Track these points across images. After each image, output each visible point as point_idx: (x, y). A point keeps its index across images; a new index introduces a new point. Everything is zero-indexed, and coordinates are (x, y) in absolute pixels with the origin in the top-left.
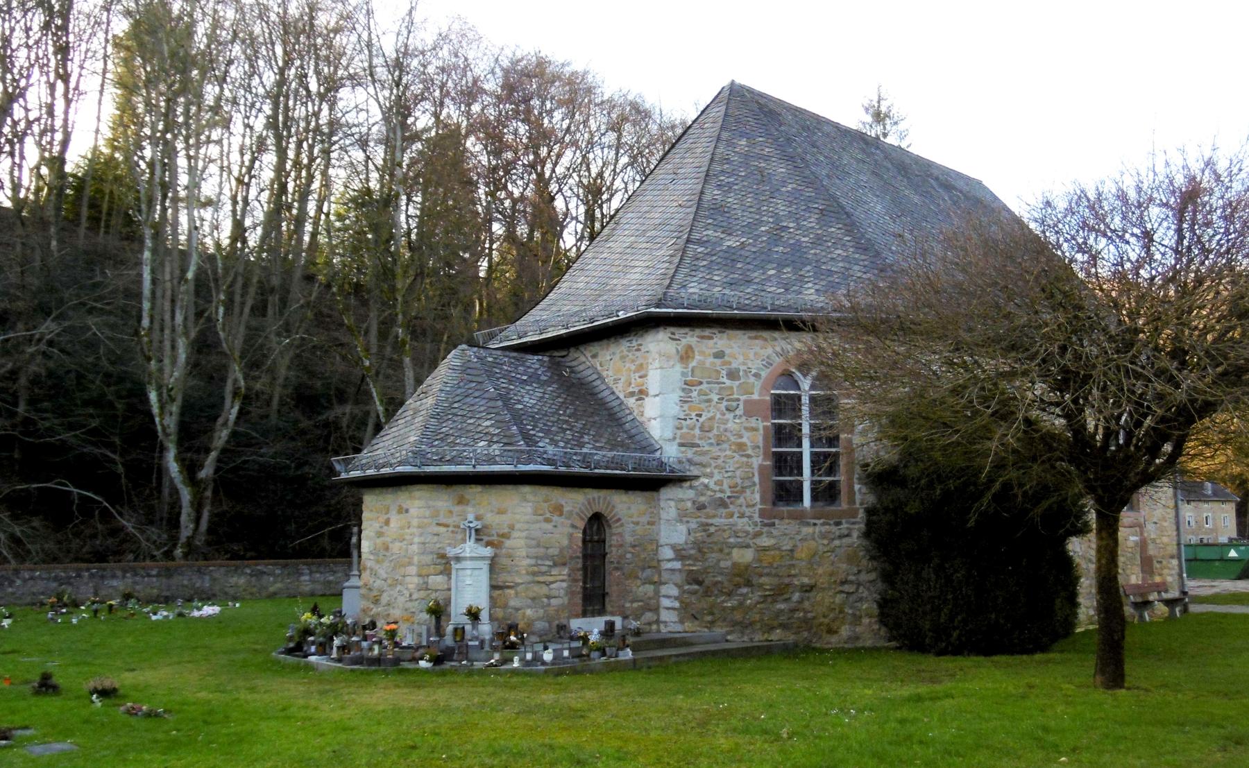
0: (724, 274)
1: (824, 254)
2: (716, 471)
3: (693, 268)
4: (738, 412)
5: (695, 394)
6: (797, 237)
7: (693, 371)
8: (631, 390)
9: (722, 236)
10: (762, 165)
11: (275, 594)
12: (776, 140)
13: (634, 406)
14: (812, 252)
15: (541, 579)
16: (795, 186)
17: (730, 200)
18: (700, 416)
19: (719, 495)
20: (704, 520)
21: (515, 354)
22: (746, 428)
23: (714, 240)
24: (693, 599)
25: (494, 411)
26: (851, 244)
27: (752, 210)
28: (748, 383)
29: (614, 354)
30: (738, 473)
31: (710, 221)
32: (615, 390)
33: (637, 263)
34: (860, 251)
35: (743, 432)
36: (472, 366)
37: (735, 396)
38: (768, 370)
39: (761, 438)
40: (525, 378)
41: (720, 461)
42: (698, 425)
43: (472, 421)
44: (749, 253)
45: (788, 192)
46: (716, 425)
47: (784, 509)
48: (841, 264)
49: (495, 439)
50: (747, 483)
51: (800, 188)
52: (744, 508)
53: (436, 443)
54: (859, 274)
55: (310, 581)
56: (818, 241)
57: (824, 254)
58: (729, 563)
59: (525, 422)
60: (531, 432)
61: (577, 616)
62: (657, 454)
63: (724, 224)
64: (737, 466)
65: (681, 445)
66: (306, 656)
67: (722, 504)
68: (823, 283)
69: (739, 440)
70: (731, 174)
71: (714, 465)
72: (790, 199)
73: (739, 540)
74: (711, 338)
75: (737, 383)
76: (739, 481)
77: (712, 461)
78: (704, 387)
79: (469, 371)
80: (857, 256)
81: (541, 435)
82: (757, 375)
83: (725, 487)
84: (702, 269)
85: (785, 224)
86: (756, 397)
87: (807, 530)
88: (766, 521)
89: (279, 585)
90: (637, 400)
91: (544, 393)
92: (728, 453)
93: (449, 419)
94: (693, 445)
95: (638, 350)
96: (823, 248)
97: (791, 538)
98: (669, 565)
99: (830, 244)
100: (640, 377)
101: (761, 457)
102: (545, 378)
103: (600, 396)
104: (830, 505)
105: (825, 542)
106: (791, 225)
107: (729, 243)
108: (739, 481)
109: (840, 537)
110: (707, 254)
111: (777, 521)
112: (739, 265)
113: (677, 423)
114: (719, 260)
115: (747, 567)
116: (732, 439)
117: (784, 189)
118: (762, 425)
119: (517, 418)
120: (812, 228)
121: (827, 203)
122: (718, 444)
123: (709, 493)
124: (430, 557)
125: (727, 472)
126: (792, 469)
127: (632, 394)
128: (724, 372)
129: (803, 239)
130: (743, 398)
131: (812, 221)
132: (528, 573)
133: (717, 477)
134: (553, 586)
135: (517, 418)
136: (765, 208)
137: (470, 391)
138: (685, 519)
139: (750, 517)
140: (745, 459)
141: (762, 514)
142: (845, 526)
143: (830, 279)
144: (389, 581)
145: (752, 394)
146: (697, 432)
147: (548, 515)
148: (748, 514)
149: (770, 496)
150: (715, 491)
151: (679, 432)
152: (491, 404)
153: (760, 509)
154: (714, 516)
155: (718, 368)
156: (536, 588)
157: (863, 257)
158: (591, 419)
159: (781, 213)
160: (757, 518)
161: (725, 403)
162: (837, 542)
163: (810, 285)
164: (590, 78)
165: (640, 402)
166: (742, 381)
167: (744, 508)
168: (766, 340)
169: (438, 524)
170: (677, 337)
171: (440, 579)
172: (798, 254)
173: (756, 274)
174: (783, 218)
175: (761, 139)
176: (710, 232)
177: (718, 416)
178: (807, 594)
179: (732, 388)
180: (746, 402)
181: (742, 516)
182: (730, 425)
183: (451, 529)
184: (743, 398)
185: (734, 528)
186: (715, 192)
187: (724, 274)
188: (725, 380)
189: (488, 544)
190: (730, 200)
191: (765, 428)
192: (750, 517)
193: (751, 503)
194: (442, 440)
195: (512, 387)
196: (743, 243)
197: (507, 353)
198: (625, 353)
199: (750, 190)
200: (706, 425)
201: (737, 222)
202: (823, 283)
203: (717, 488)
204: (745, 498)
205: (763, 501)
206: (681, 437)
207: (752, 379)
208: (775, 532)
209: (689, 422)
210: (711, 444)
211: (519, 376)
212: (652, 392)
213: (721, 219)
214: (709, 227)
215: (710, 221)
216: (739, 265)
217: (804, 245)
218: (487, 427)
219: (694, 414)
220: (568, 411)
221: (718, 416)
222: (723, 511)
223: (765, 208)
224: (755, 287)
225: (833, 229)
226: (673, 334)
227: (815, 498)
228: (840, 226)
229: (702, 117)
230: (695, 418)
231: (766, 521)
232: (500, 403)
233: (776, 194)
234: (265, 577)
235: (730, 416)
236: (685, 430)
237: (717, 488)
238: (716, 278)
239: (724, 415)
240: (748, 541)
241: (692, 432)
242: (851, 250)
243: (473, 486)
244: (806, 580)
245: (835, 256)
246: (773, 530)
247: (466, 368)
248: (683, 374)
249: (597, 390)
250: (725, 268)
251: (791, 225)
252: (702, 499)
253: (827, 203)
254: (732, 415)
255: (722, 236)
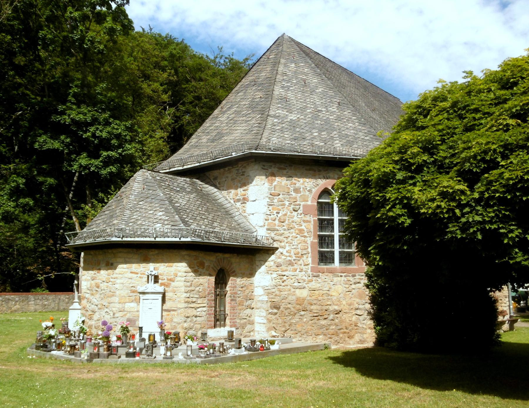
0: (290, 134)
1: (342, 125)
2: (287, 245)
3: (273, 130)
4: (299, 212)
5: (276, 201)
6: (327, 116)
7: (275, 187)
8: (238, 198)
9: (287, 113)
10: (304, 78)
11: (15, 311)
12: (310, 65)
13: (240, 207)
14: (336, 124)
15: (192, 305)
16: (323, 89)
17: (289, 95)
18: (278, 213)
19: (289, 258)
20: (280, 272)
21: (171, 176)
22: (304, 221)
23: (282, 115)
24: (274, 317)
25: (164, 207)
26: (357, 121)
27: (302, 101)
28: (305, 195)
29: (227, 177)
30: (299, 246)
31: (279, 105)
32: (228, 198)
33: (238, 128)
34: (362, 125)
35: (302, 223)
36: (148, 181)
37: (298, 203)
38: (316, 188)
39: (312, 227)
40: (178, 189)
41: (289, 239)
42: (278, 218)
43: (151, 212)
44: (303, 123)
45: (320, 92)
46: (287, 218)
47: (323, 267)
48: (352, 131)
49: (166, 222)
50: (304, 252)
51: (326, 90)
52: (302, 266)
53: (131, 224)
54: (363, 137)
55: (34, 304)
56: (339, 119)
57: (342, 125)
58: (294, 298)
59: (182, 213)
60: (186, 219)
61: (211, 328)
62: (255, 234)
63: (288, 107)
64: (299, 242)
65: (268, 229)
66: (50, 351)
67: (291, 263)
68: (345, 141)
69: (300, 228)
70: (288, 82)
71: (286, 241)
72: (321, 96)
73: (300, 284)
74: (285, 169)
75: (299, 195)
76: (299, 250)
77: (285, 239)
78: (281, 196)
79: (147, 184)
80: (360, 127)
81: (192, 221)
82: (310, 191)
83: (292, 253)
84: (278, 131)
85: (320, 109)
86: (309, 203)
87: (336, 279)
88: (315, 274)
89: (18, 306)
90: (242, 204)
91: (189, 198)
92: (294, 234)
93: (137, 211)
94: (274, 230)
95: (243, 175)
96: (342, 122)
97: (328, 284)
98: (260, 298)
99: (345, 120)
100: (244, 191)
101: (312, 238)
102: (189, 190)
103: (219, 201)
104: (348, 265)
105: (347, 286)
106: (323, 109)
107: (291, 118)
108: (299, 250)
109: (355, 283)
110: (279, 123)
111: (320, 274)
112: (298, 130)
113: (266, 217)
114: (286, 127)
115: (304, 299)
116: (296, 226)
117: (317, 91)
118: (313, 219)
119: (178, 211)
120: (335, 111)
121: (341, 99)
122: (288, 230)
123: (283, 257)
124: (127, 291)
125: (293, 245)
126: (328, 245)
127: (238, 200)
128: (292, 189)
129: (331, 117)
130: (302, 203)
131: (334, 108)
132: (186, 302)
133: (288, 248)
134: (198, 310)
135: (178, 211)
136: (308, 100)
137: (149, 195)
138: (270, 272)
139: (306, 272)
140: (303, 238)
141: (313, 269)
142: (357, 277)
143: (347, 139)
144: (99, 306)
145: (307, 201)
146: (277, 222)
147: (197, 268)
148: (304, 270)
149: (317, 260)
150: (287, 256)
151: (267, 222)
152: (162, 202)
153: (311, 267)
154: (286, 270)
155: (289, 186)
156: (190, 310)
157: (363, 128)
158: (216, 214)
159: (317, 103)
160: (309, 272)
161: (292, 206)
162: (353, 286)
163: (337, 142)
164: (185, 42)
165: (243, 205)
166: (302, 194)
167: (302, 266)
168: (315, 171)
169: (131, 272)
170: (266, 168)
171: (133, 305)
172: (329, 125)
173: (307, 135)
174: (318, 106)
175: (302, 64)
176: (280, 111)
177: (289, 213)
178: (337, 315)
179: (296, 198)
180: (304, 206)
181: (301, 271)
182: (295, 219)
183: (139, 275)
184: (302, 203)
185: (297, 278)
186: (281, 90)
187: (290, 134)
188: (292, 193)
189: (162, 284)
190: (289, 95)
191: (314, 220)
192: (306, 272)
193: (306, 263)
194: (134, 222)
195: (172, 194)
196: (298, 118)
197: (167, 175)
198: (235, 176)
199: (299, 90)
200: (282, 218)
201: (294, 107)
202: (345, 141)
203: (288, 254)
204: (303, 261)
205: (313, 262)
206: (268, 225)
207: (307, 193)
208: (319, 280)
209: (272, 216)
210: (285, 230)
211: (175, 188)
212: (251, 198)
213: (285, 104)
214: (279, 108)
215: (279, 105)
216: (298, 130)
217: (331, 120)
218: (160, 216)
219: (275, 212)
220: (204, 209)
221: (289, 213)
222: (290, 268)
223: (308, 100)
224: (308, 141)
225: (346, 113)
226: (264, 166)
227: (341, 261)
228: (350, 111)
229: (268, 53)
230: (276, 214)
231: (315, 274)
232: (167, 202)
233: (313, 93)
234: (11, 302)
235: (295, 213)
236: (270, 221)
237: (288, 254)
238: (286, 136)
239: (292, 213)
240: (305, 284)
241: (274, 222)
242: (357, 124)
243: (153, 250)
244: (336, 307)
245: (349, 127)
246: (318, 279)
247: (145, 181)
248: (269, 189)
249: (217, 198)
250: (290, 130)
251: (323, 109)
252: (279, 260)
253: (341, 99)
254: (296, 213)
255: (287, 113)
